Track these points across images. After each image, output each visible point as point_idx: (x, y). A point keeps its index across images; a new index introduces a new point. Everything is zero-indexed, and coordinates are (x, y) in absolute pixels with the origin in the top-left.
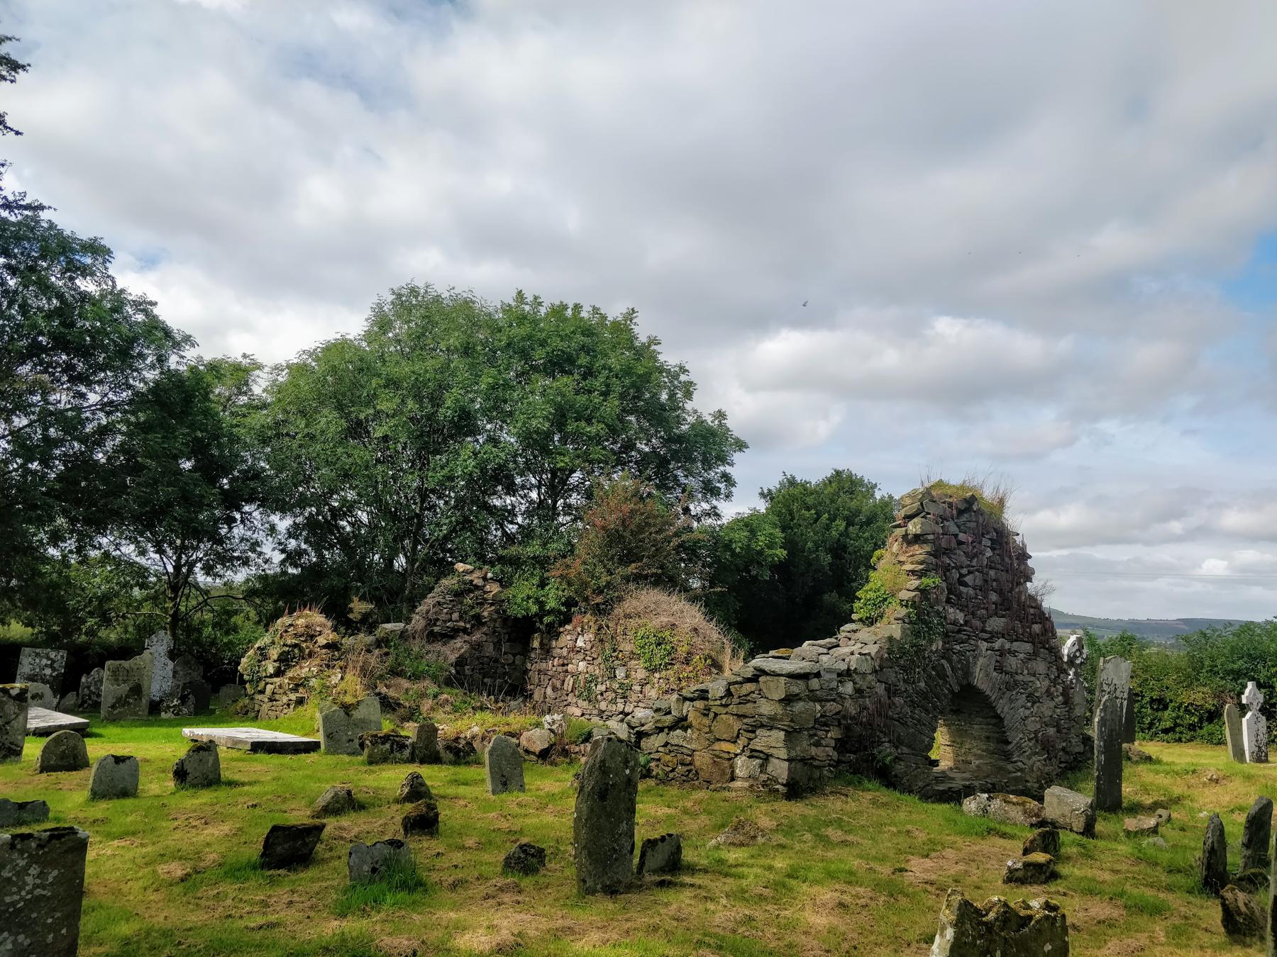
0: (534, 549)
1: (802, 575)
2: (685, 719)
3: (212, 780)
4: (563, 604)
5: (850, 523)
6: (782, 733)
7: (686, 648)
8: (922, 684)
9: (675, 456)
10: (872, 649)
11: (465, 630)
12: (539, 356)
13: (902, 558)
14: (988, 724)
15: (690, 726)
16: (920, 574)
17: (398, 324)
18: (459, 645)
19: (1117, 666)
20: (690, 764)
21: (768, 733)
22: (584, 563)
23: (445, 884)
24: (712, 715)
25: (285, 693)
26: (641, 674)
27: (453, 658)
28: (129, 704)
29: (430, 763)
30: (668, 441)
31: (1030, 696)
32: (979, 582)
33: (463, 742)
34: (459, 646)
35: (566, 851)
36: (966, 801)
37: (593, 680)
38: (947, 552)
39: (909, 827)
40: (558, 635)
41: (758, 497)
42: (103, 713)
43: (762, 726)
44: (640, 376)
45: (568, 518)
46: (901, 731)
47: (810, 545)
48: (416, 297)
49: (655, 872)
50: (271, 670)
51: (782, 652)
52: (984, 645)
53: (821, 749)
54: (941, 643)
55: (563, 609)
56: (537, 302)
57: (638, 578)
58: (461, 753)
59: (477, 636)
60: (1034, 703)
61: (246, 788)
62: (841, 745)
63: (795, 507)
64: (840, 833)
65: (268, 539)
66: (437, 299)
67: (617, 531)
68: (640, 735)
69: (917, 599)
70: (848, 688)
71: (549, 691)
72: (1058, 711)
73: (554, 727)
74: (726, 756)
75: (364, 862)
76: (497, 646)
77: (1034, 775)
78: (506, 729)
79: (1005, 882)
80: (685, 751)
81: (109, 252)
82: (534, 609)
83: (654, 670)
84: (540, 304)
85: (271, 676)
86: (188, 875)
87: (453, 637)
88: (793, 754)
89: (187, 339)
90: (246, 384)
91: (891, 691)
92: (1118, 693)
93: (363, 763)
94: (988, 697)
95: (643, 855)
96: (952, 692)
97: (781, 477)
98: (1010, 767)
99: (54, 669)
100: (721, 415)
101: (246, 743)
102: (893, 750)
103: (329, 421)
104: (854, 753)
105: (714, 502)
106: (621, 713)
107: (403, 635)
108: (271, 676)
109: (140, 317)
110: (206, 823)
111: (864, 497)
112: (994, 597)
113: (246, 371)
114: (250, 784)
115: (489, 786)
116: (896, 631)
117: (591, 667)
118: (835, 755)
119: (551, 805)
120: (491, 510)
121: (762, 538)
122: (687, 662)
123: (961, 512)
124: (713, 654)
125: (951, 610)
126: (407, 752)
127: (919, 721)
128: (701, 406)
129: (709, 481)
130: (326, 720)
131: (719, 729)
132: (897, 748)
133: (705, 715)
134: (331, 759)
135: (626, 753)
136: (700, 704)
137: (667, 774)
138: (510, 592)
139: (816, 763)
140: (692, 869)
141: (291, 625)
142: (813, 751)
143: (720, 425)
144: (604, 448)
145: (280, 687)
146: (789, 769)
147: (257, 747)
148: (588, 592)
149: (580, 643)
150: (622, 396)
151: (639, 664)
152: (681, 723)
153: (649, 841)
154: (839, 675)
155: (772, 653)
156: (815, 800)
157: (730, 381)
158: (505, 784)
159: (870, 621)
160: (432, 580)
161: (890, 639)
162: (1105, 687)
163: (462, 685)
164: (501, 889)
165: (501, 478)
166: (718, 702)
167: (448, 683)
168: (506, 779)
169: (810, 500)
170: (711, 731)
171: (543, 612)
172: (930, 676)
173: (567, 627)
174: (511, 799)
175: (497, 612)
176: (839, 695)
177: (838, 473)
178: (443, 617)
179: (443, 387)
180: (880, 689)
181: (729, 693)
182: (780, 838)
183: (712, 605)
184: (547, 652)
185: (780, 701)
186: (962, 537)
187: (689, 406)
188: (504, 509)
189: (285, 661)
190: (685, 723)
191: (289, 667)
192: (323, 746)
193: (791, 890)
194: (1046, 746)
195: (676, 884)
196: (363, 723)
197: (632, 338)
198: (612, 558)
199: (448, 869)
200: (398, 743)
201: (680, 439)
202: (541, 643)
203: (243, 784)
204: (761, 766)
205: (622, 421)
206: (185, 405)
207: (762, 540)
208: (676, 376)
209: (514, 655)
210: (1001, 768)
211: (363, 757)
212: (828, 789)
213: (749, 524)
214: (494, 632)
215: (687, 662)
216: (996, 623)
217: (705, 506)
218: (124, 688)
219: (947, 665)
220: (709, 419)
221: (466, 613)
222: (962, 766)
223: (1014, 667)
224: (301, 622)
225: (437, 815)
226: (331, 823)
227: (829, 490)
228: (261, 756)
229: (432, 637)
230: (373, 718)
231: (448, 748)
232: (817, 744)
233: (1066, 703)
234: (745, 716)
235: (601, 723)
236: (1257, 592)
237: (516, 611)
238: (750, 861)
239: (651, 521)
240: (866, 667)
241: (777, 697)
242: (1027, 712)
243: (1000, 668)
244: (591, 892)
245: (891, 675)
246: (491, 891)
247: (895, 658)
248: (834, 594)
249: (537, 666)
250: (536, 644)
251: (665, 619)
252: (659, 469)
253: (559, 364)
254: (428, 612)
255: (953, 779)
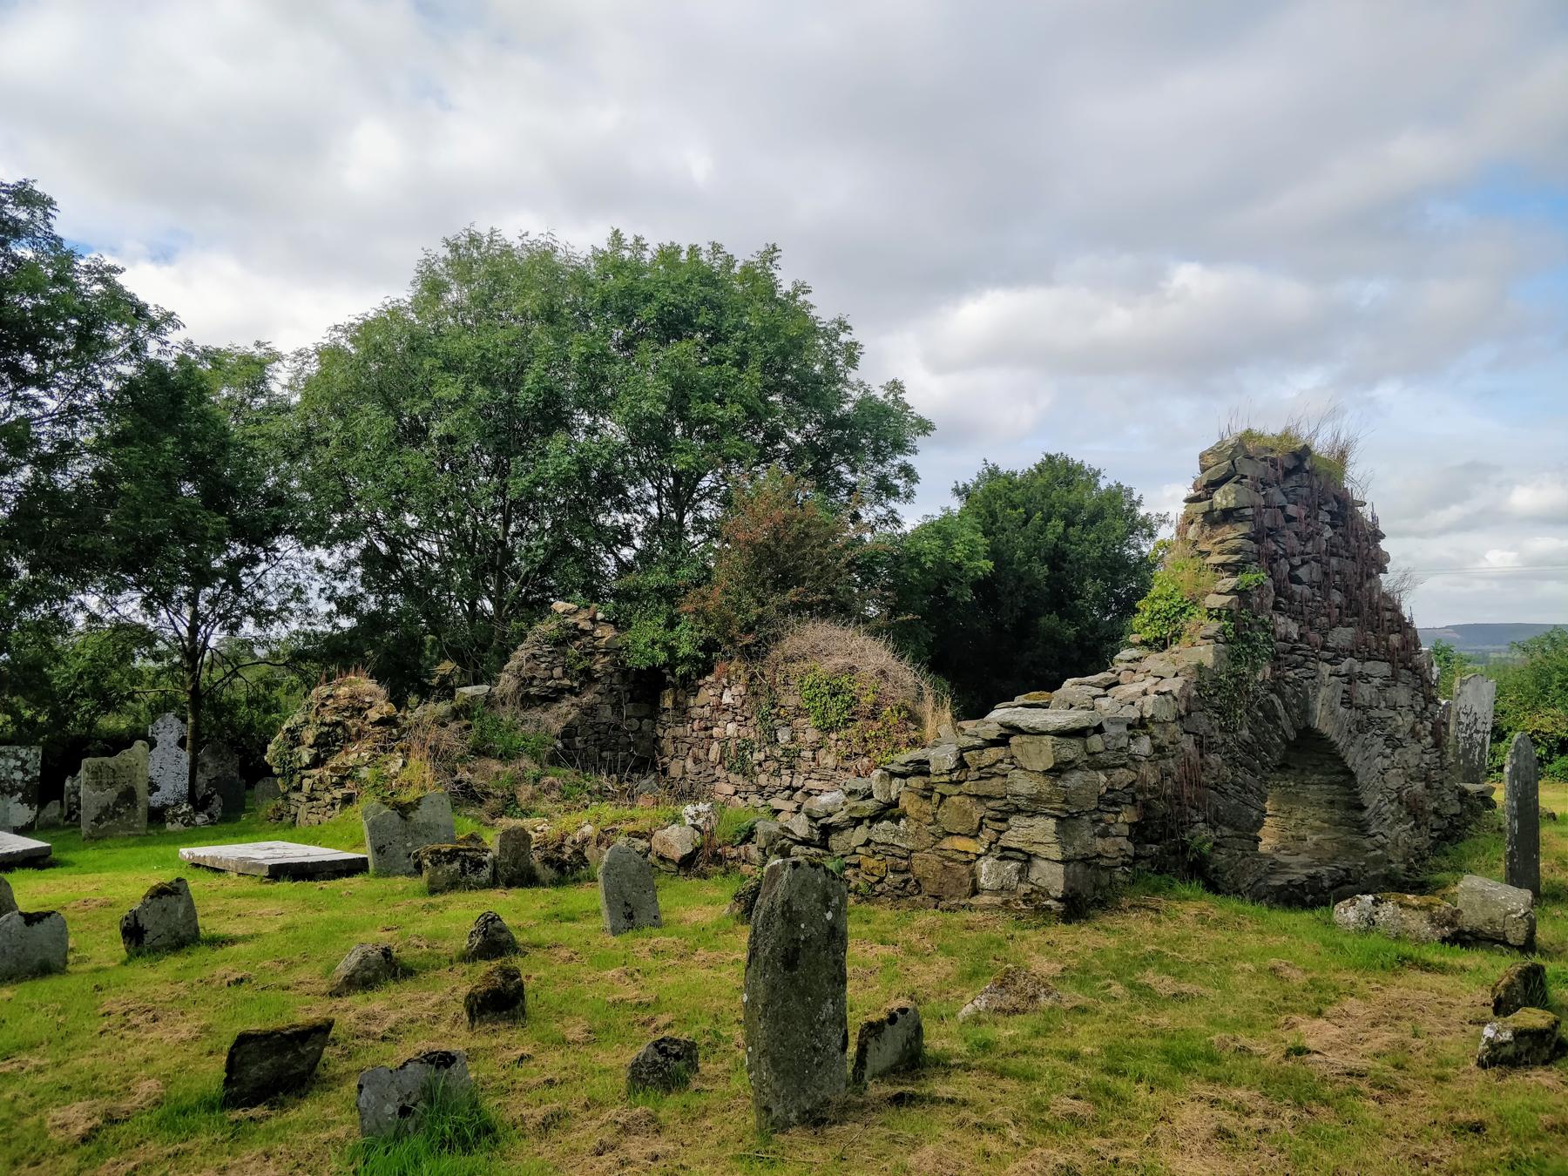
0: (658, 577)
1: (1011, 593)
2: (895, 804)
3: (185, 939)
4: (700, 649)
5: (1070, 523)
6: (1052, 822)
7: (871, 698)
8: (1245, 733)
9: (837, 445)
10: (1174, 685)
11: (571, 690)
12: (648, 312)
13: (1204, 547)
14: (1331, 783)
15: (903, 815)
16: (1235, 569)
17: (454, 287)
18: (564, 710)
19: (1477, 689)
20: (907, 871)
21: (1029, 822)
22: (727, 593)
23: (530, 1124)
24: (936, 798)
25: (327, 789)
26: (812, 735)
27: (557, 728)
28: (120, 815)
29: (521, 886)
30: (830, 424)
31: (1389, 738)
32: (1317, 576)
33: (568, 851)
34: (565, 711)
35: (730, 1039)
36: (1339, 908)
37: (748, 746)
38: (1272, 533)
39: (1274, 962)
40: (696, 691)
41: (949, 493)
42: (84, 830)
43: (1018, 811)
44: (790, 340)
45: (700, 537)
46: (1221, 803)
47: (1020, 554)
48: (478, 248)
49: (882, 1075)
50: (306, 759)
51: (1034, 696)
52: (1326, 669)
53: (1109, 840)
54: (1268, 670)
55: (701, 655)
56: (639, 244)
57: (797, 608)
58: (566, 867)
59: (588, 698)
60: (1395, 748)
61: (240, 947)
62: (1138, 833)
63: (997, 506)
64: (1168, 980)
65: (306, 584)
66: (507, 251)
67: (768, 547)
68: (827, 830)
69: (1234, 606)
70: (1144, 746)
71: (689, 763)
72: (1427, 757)
73: (699, 822)
74: (963, 858)
75: (385, 1099)
76: (617, 707)
77: (1399, 852)
78: (631, 827)
79: (1482, 1065)
80: (897, 851)
81: (50, 202)
82: (662, 657)
83: (830, 729)
84: (644, 247)
85: (307, 767)
86: (97, 1129)
87: (556, 700)
88: (1070, 852)
89: (169, 318)
90: (263, 381)
91: (1203, 745)
92: (1479, 726)
93: (422, 893)
94: (1333, 744)
95: (862, 1050)
96: (1286, 740)
97: (980, 467)
98: (1367, 843)
99: (26, 772)
100: (896, 387)
101: (262, 866)
102: (1210, 833)
103: (373, 421)
104: (1155, 842)
105: (892, 504)
106: (788, 788)
107: (489, 701)
108: (307, 767)
109: (98, 288)
110: (155, 1019)
111: (1086, 487)
112: (1337, 597)
113: (262, 365)
114: (245, 939)
115: (605, 921)
116: (1206, 654)
117: (743, 731)
118: (1129, 847)
119: (703, 961)
120: (599, 530)
121: (960, 547)
122: (874, 716)
123: (1288, 473)
124: (909, 703)
125: (1281, 620)
126: (486, 873)
127: (1243, 786)
128: (869, 377)
129: (885, 477)
130: (373, 827)
131: (948, 817)
132: (1215, 829)
133: (925, 797)
134: (381, 885)
135: (825, 884)
136: (916, 782)
137: (871, 886)
138: (628, 637)
139: (1104, 862)
140: (942, 1065)
141: (329, 696)
142: (1100, 844)
143: (896, 401)
144: (742, 439)
145: (321, 780)
146: (1066, 874)
147: (279, 872)
148: (734, 631)
149: (727, 699)
150: (765, 367)
151: (822, 733)
152: (889, 811)
153: (870, 1025)
154: (1130, 727)
155: (1020, 699)
156: (1106, 920)
157: (897, 359)
158: (630, 916)
159: (1161, 644)
160: (523, 625)
161: (1200, 668)
162: (1463, 718)
163: (572, 762)
164: (625, 1129)
165: (609, 488)
166: (946, 778)
167: (554, 760)
168: (631, 912)
169: (1017, 496)
170: (936, 822)
171: (672, 664)
172: (1255, 720)
173: (708, 678)
174: (639, 945)
175: (613, 663)
176: (1132, 757)
177: (1050, 458)
178: (540, 674)
179: (521, 369)
180: (1188, 743)
181: (962, 764)
182: (1073, 996)
183: (901, 638)
184: (682, 712)
185: (1047, 772)
186: (1292, 510)
187: (853, 376)
188: (616, 530)
189: (327, 744)
190: (896, 811)
191: (332, 753)
192: (371, 867)
193: (1121, 1100)
194: (1414, 810)
195: (922, 1099)
196: (427, 830)
197: (772, 289)
198: (763, 584)
199: (538, 1086)
200: (471, 860)
201: (843, 423)
202: (675, 701)
203: (233, 941)
204: (1020, 871)
205: (764, 400)
206: (169, 406)
207: (960, 550)
208: (832, 336)
209: (640, 719)
210: (1352, 846)
211: (422, 882)
212: (1125, 902)
213: (940, 530)
214: (611, 690)
215: (874, 716)
216: (1342, 636)
217: (881, 511)
218: (110, 795)
219: (1277, 701)
220: (880, 394)
221: (571, 667)
222: (1291, 844)
223: (1367, 698)
224: (343, 691)
225: (520, 987)
226: (349, 1012)
227: (1041, 481)
228: (285, 886)
229: (528, 701)
230: (441, 821)
231: (547, 861)
232: (1104, 834)
233: (1437, 745)
234: (989, 798)
235: (761, 802)
236: (1551, 588)
237: (637, 662)
238: (1038, 1043)
239: (813, 531)
240: (1166, 713)
241: (1040, 767)
242: (1387, 763)
243: (1348, 702)
244: (783, 1126)
245: (1202, 722)
246: (607, 1135)
247: (1209, 696)
248: (1054, 616)
249: (669, 733)
250: (668, 703)
251: (840, 661)
252: (817, 464)
253: (673, 326)
254: (520, 668)
255: (1286, 865)
